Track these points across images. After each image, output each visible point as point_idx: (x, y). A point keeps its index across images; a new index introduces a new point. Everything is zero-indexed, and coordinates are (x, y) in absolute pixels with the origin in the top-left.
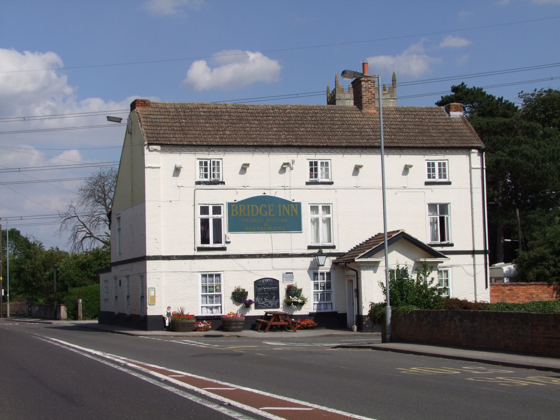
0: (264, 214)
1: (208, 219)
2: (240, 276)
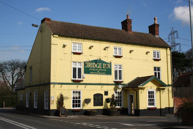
0: (98, 67)
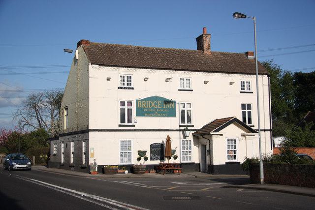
0: (156, 106)
1: (125, 109)
2: (143, 142)
